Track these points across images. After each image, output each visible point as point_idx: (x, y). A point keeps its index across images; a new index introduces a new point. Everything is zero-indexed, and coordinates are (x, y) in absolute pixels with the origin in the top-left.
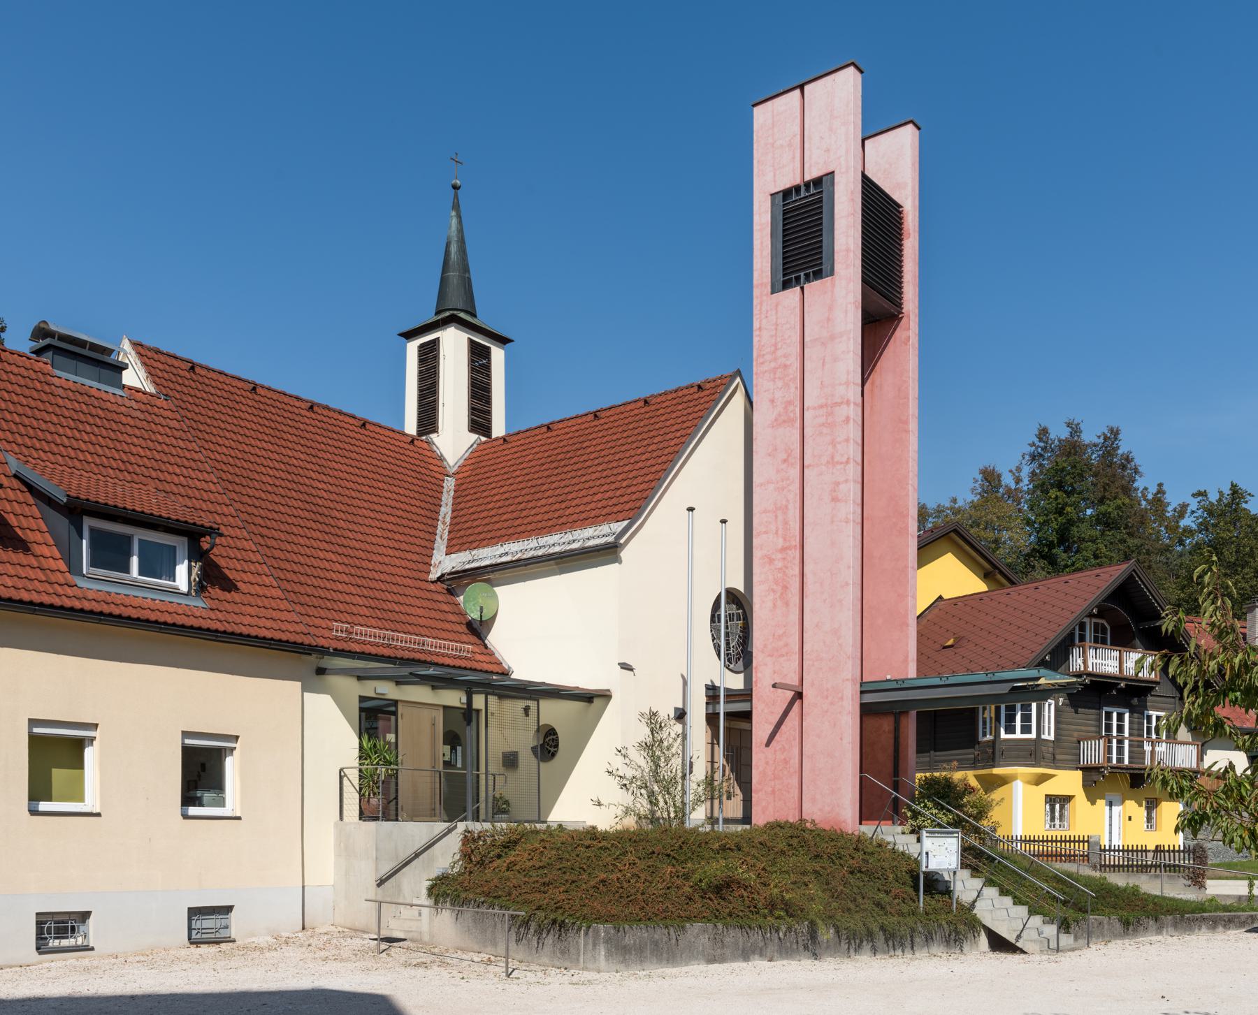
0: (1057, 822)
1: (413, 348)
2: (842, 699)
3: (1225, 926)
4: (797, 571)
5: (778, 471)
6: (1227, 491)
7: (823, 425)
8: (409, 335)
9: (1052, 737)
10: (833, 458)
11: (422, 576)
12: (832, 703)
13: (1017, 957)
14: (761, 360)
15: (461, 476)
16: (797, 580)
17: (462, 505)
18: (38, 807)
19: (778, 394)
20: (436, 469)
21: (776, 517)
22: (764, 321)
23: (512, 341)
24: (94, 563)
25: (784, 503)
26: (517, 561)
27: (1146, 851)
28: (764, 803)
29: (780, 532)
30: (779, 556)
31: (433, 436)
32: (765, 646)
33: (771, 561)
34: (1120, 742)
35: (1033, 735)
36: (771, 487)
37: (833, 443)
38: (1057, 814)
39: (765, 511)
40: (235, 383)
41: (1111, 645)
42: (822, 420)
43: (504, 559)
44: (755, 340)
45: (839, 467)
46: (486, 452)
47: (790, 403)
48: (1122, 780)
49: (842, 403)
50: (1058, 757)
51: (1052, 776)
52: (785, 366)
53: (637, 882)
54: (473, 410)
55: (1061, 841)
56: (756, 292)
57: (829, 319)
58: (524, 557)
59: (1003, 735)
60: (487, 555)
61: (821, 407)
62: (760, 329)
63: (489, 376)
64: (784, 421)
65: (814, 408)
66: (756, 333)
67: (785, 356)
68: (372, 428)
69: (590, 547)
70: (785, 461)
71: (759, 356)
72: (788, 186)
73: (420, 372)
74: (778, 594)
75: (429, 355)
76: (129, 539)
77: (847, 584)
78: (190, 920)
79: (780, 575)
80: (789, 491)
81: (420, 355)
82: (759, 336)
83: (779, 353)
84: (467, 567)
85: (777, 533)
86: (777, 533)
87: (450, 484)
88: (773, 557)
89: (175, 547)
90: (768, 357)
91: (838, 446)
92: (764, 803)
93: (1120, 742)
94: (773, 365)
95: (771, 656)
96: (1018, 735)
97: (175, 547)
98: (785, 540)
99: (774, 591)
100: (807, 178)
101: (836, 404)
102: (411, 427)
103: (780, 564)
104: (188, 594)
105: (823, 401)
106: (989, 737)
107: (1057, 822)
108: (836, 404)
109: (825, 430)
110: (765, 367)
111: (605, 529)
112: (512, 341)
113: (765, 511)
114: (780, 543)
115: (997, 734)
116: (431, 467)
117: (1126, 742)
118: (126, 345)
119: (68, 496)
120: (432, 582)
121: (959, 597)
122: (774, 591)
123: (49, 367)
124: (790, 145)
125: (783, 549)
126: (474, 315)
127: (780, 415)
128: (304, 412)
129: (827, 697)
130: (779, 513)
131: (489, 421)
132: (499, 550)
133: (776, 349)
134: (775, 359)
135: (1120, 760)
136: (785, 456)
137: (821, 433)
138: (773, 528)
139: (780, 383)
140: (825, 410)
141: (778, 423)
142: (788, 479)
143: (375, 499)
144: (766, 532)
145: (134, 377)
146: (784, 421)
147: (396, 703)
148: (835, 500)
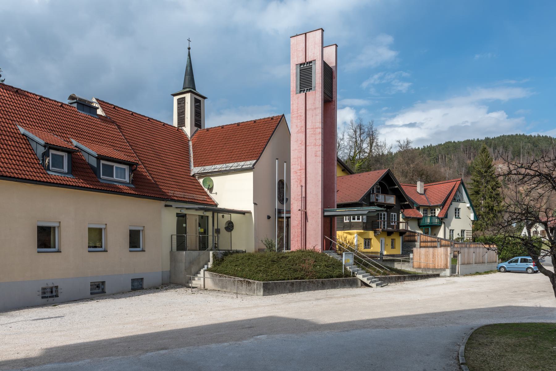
0: (367, 247)
1: (176, 98)
2: (318, 214)
3: (421, 278)
4: (304, 176)
5: (299, 147)
6: (406, 141)
7: (312, 134)
8: (174, 95)
9: (366, 221)
10: (315, 144)
11: (188, 174)
12: (315, 215)
13: (371, 288)
14: (293, 113)
15: (193, 141)
16: (304, 179)
17: (196, 151)
18: (394, 266)
19: (299, 124)
20: (185, 138)
21: (298, 160)
22: (294, 102)
23: (207, 98)
24: (103, 175)
25: (300, 156)
26: (220, 171)
27: (378, 253)
28: (294, 244)
29: (299, 165)
30: (299, 171)
31: (183, 128)
32: (295, 198)
33: (296, 173)
34: (384, 222)
35: (361, 221)
36: (297, 151)
37: (315, 139)
38: (367, 244)
39: (294, 158)
40: (126, 112)
41: (381, 193)
42: (312, 132)
43: (215, 170)
44: (291, 107)
45: (317, 146)
46: (201, 134)
47: (302, 127)
48: (485, 260)
49: (318, 128)
50: (367, 227)
51: (366, 233)
52: (301, 116)
53: (243, 270)
54: (196, 120)
55: (371, 253)
56: (291, 93)
57: (314, 103)
58: (222, 170)
59: (352, 221)
60: (209, 168)
61: (312, 128)
62: (293, 104)
63: (200, 109)
64: (300, 132)
65: (310, 129)
66: (291, 105)
67: (301, 113)
68: (166, 125)
69: (244, 168)
70: (301, 144)
71: (292, 112)
72: (301, 63)
73: (178, 107)
74: (298, 183)
75: (181, 102)
76: (112, 166)
77: (320, 181)
78: (501, 272)
79: (299, 177)
80: (302, 153)
81: (178, 102)
82: (293, 106)
83: (299, 112)
84: (203, 172)
85: (298, 165)
86: (298, 165)
87: (191, 143)
88: (297, 172)
89: (125, 169)
90: (295, 113)
91: (317, 140)
92: (294, 244)
93: (384, 222)
94: (297, 115)
95: (297, 201)
96: (356, 221)
97: (125, 169)
98: (301, 167)
99: (297, 181)
100: (307, 61)
101: (316, 128)
102: (175, 124)
103: (299, 174)
104: (129, 183)
105: (312, 127)
106: (347, 221)
107: (367, 247)
108: (316, 128)
109: (313, 135)
110: (294, 116)
111: (248, 162)
112: (207, 98)
113: (294, 158)
114: (299, 168)
115: (350, 220)
116: (184, 138)
117: (386, 222)
118: (94, 100)
119: (98, 154)
120: (192, 176)
121: (231, 124)
122: (297, 181)
123: (76, 109)
124: (302, 50)
125: (301, 170)
126: (195, 90)
127: (299, 130)
128: (147, 121)
129: (314, 213)
130: (299, 159)
131: (201, 123)
132: (214, 167)
133: (298, 111)
134: (298, 113)
135: (384, 228)
136: (301, 142)
137: (312, 136)
138: (297, 163)
139: (299, 121)
140: (313, 130)
141: (298, 132)
142: (302, 149)
143: (171, 149)
144: (295, 164)
145: (100, 112)
146: (300, 132)
147: (186, 214)
148: (316, 156)
